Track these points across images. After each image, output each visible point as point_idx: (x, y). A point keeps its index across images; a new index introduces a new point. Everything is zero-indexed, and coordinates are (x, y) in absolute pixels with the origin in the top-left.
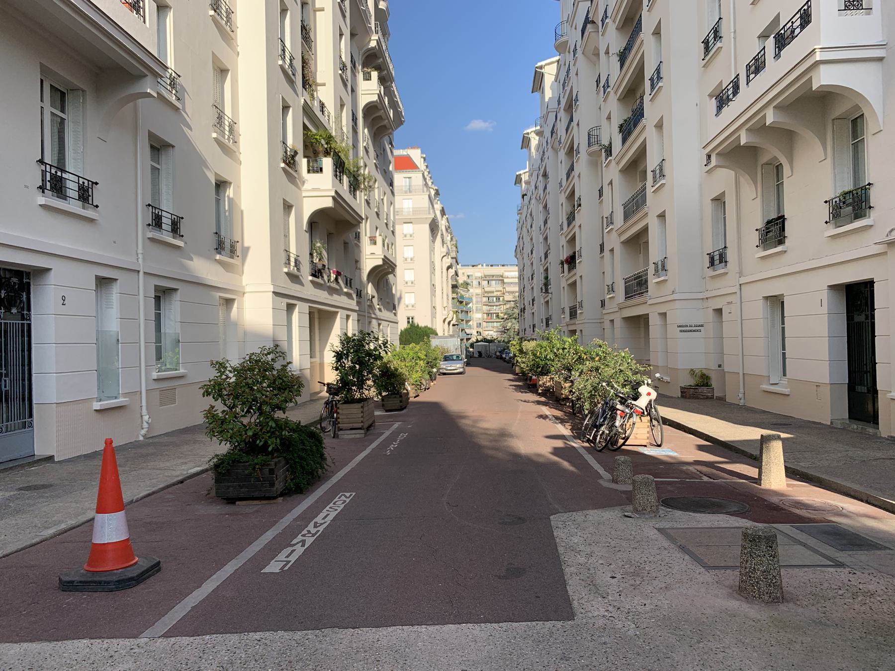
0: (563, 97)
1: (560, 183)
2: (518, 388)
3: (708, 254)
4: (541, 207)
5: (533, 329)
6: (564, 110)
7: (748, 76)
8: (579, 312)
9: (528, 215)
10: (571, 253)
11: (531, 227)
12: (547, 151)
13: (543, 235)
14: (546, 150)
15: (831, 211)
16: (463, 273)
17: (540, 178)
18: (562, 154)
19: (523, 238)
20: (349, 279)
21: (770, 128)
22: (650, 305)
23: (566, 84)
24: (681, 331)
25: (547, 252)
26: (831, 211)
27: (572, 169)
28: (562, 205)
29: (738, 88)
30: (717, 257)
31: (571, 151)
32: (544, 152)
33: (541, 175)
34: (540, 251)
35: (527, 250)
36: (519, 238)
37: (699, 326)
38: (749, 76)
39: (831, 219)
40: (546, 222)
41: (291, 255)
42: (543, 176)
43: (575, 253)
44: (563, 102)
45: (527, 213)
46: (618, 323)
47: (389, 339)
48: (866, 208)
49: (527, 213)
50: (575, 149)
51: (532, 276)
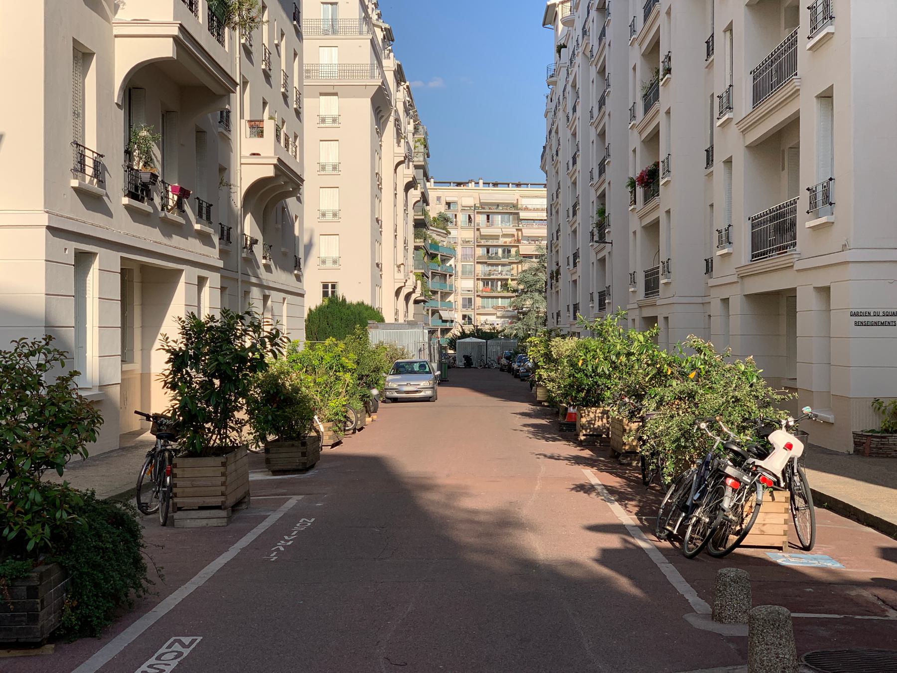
4: (593, 71)
9: (569, 88)
16: (439, 198)
17: (594, 13)
19: (557, 132)
35: (565, 156)
42: (598, 9)
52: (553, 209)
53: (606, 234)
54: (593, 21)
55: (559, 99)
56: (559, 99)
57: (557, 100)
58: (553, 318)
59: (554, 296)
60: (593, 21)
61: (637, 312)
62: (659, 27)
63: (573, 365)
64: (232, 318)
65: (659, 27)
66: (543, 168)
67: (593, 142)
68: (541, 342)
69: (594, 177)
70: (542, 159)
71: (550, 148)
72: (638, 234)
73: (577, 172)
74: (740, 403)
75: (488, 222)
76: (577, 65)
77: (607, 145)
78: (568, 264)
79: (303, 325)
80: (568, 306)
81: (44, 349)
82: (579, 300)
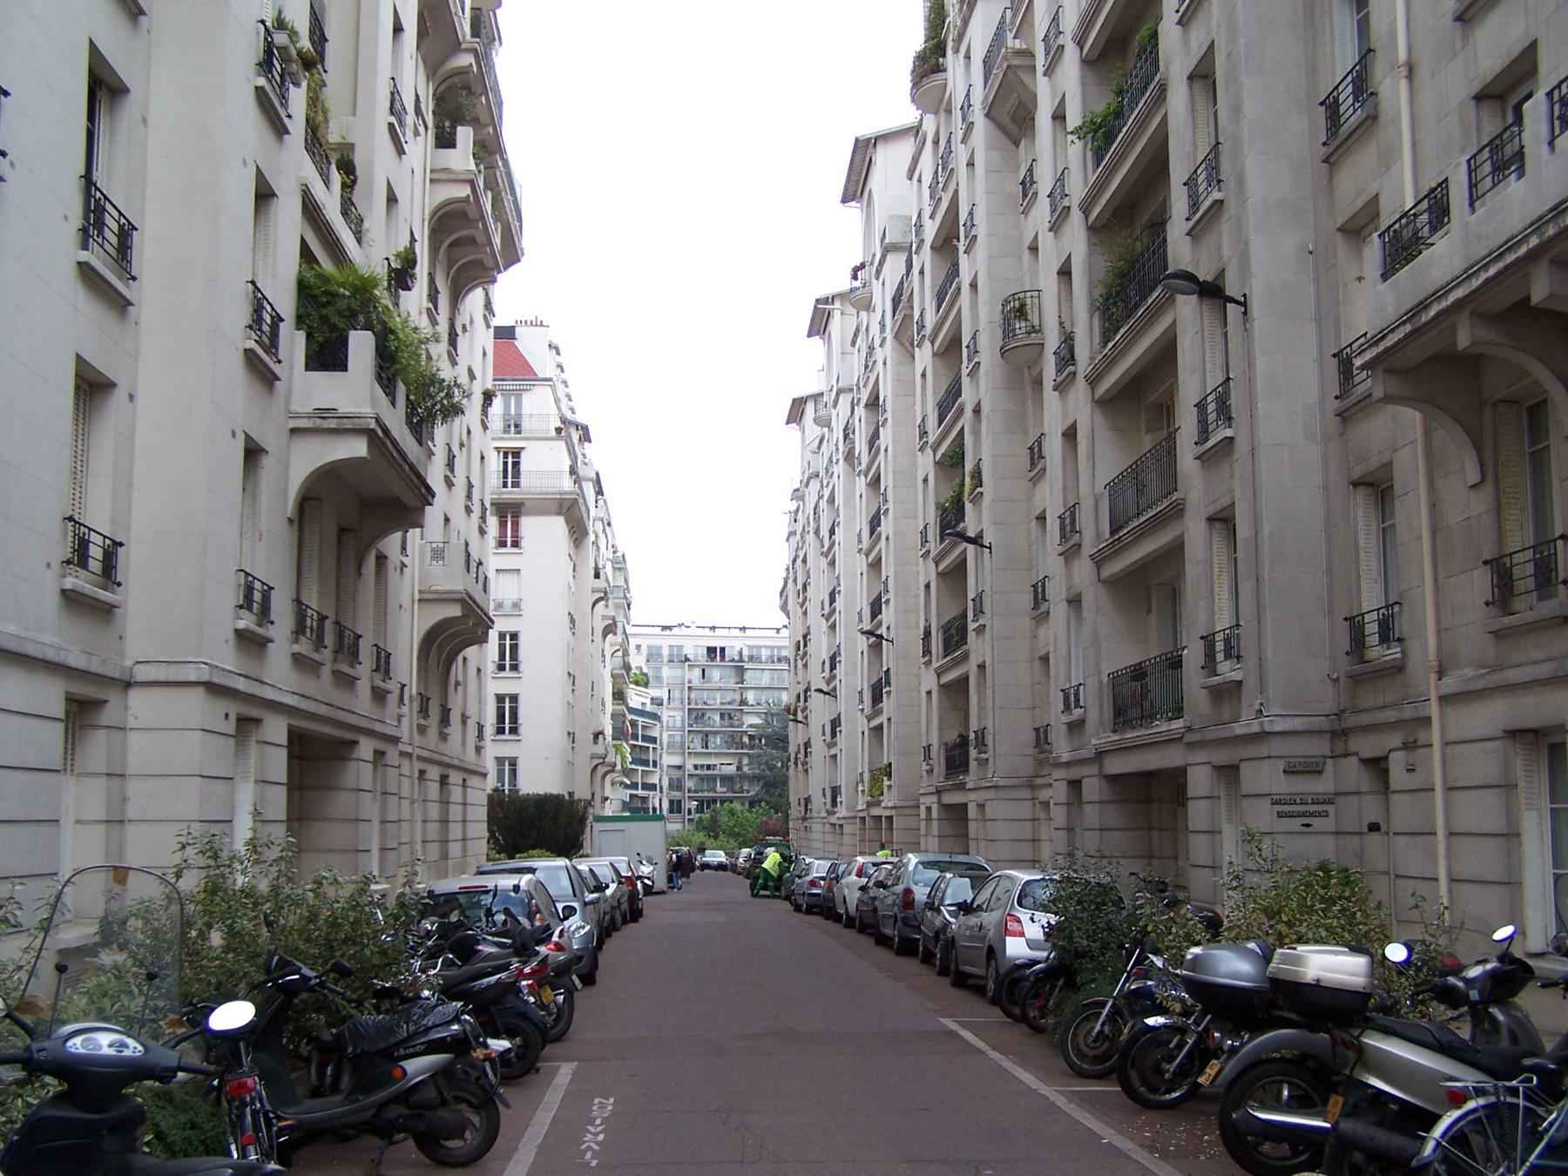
0: (932, 217)
1: (924, 434)
2: (1047, 622)
3: (1346, 619)
4: (861, 484)
5: (806, 806)
6: (932, 247)
7: (1473, 185)
8: (972, 626)
9: (823, 504)
10: (951, 613)
11: (832, 532)
12: (881, 346)
13: (867, 555)
14: (877, 343)
15: (1495, 583)
16: (638, 647)
17: (860, 411)
18: (924, 357)
19: (804, 561)
20: (383, 654)
21: (1540, 313)
22: (1188, 743)
23: (941, 186)
24: (1280, 815)
25: (879, 597)
26: (1495, 583)
27: (954, 391)
28: (925, 480)
29: (1446, 211)
30: (1372, 628)
31: (951, 350)
32: (871, 348)
33: (862, 404)
34: (856, 598)
35: (818, 593)
36: (794, 561)
37: (1324, 803)
38: (1476, 185)
39: (1496, 597)
40: (875, 523)
41: (310, 612)
42: (866, 406)
43: (964, 740)
44: (930, 230)
45: (821, 497)
46: (1092, 788)
47: (990, 725)
48: (1558, 584)
49: (821, 497)
50: (964, 345)
51: (805, 637)
52: (799, 661)
53: (885, 695)
54: (885, 364)
55: (836, 445)
56: (836, 445)
57: (805, 521)
58: (799, 804)
59: (801, 775)
60: (885, 364)
61: (934, 798)
62: (963, 427)
63: (257, 936)
64: (673, 888)
65: (963, 427)
66: (784, 608)
67: (925, 480)
68: (172, 1116)
69: (864, 620)
70: (781, 596)
71: (795, 580)
72: (935, 695)
73: (837, 613)
74: (1099, 943)
75: (703, 678)
76: (835, 476)
77: (883, 579)
78: (824, 734)
79: (485, 801)
80: (824, 789)
81: (642, 882)
82: (843, 781)
